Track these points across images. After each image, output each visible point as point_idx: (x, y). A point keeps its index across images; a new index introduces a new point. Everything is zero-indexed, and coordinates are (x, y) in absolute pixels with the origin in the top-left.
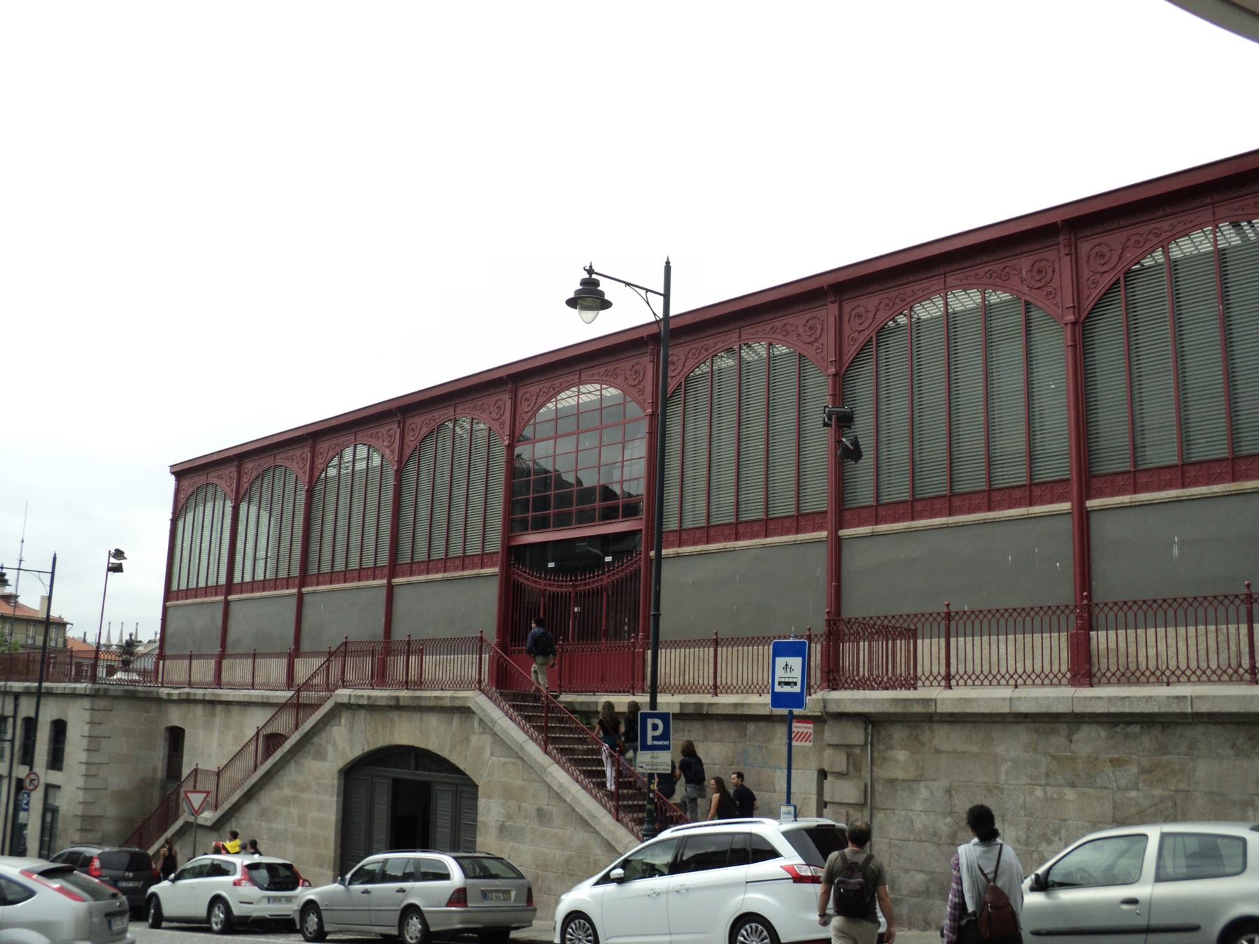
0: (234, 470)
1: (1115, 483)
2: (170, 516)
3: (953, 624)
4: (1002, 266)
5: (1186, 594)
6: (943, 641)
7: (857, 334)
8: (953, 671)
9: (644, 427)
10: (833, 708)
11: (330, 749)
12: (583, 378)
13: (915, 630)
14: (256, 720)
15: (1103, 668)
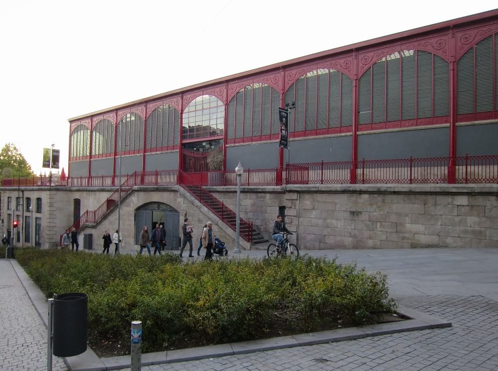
0: (180, 98)
1: (467, 117)
2: (69, 135)
3: (324, 166)
4: (425, 42)
5: (373, 160)
6: (409, 169)
7: (232, 94)
8: (324, 179)
9: (223, 108)
10: (288, 189)
11: (132, 204)
12: (204, 93)
13: (308, 168)
14: (105, 196)
15: (359, 179)
